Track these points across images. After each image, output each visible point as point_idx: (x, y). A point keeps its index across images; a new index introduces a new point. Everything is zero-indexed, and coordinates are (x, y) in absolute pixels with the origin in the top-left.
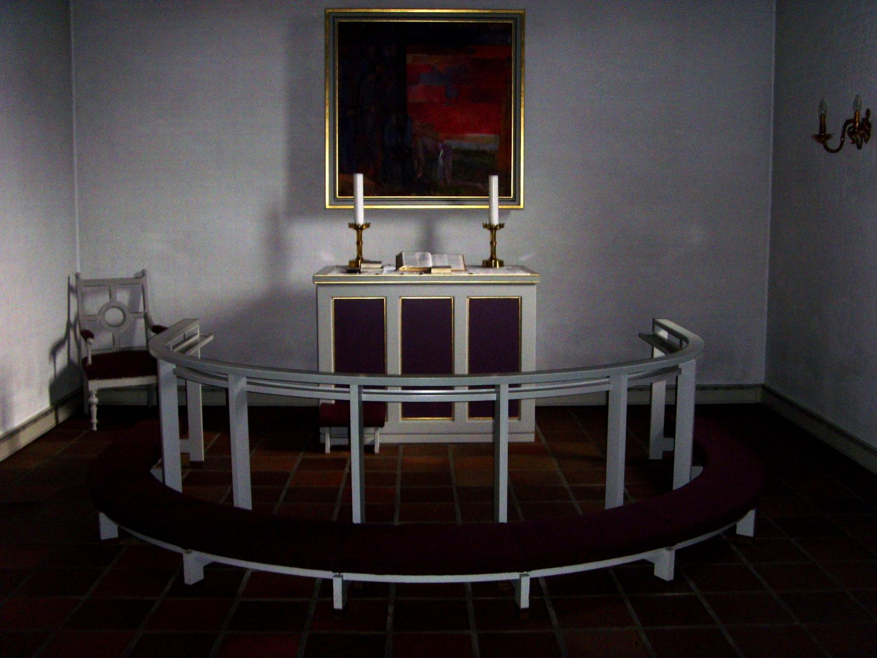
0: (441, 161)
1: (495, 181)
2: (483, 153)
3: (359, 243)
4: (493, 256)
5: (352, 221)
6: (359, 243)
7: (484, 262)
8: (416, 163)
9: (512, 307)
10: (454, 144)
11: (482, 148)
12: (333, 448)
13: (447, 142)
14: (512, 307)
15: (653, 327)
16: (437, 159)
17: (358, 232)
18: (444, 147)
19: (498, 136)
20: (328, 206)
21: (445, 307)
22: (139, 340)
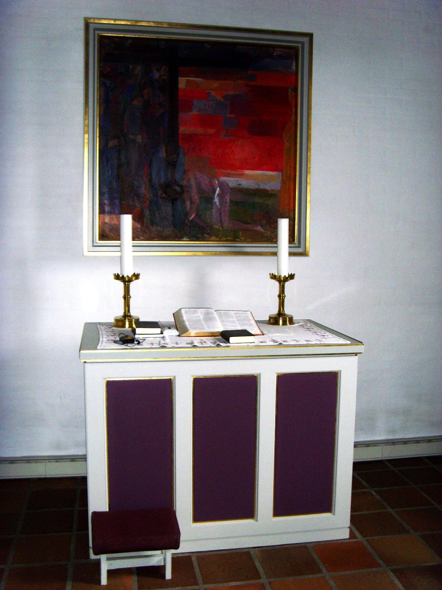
0: (216, 200)
1: (284, 225)
2: (264, 193)
3: (127, 297)
4: (281, 314)
5: (118, 271)
6: (127, 297)
7: (270, 318)
8: (188, 203)
9: (328, 382)
10: (232, 181)
11: (262, 187)
12: (110, 573)
13: (223, 179)
14: (328, 382)
15: (262, 332)
16: (213, 198)
17: (125, 284)
18: (222, 185)
19: (280, 174)
20: (86, 253)
21: (247, 386)
22: (111, 227)
